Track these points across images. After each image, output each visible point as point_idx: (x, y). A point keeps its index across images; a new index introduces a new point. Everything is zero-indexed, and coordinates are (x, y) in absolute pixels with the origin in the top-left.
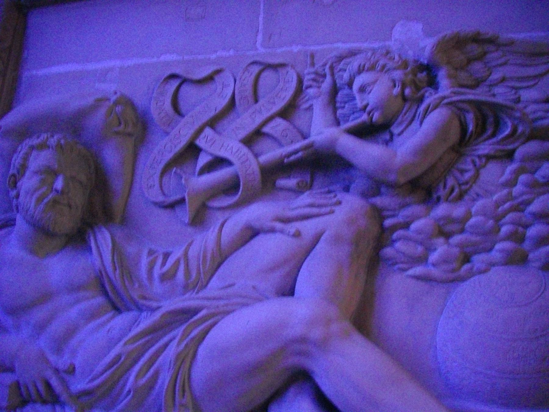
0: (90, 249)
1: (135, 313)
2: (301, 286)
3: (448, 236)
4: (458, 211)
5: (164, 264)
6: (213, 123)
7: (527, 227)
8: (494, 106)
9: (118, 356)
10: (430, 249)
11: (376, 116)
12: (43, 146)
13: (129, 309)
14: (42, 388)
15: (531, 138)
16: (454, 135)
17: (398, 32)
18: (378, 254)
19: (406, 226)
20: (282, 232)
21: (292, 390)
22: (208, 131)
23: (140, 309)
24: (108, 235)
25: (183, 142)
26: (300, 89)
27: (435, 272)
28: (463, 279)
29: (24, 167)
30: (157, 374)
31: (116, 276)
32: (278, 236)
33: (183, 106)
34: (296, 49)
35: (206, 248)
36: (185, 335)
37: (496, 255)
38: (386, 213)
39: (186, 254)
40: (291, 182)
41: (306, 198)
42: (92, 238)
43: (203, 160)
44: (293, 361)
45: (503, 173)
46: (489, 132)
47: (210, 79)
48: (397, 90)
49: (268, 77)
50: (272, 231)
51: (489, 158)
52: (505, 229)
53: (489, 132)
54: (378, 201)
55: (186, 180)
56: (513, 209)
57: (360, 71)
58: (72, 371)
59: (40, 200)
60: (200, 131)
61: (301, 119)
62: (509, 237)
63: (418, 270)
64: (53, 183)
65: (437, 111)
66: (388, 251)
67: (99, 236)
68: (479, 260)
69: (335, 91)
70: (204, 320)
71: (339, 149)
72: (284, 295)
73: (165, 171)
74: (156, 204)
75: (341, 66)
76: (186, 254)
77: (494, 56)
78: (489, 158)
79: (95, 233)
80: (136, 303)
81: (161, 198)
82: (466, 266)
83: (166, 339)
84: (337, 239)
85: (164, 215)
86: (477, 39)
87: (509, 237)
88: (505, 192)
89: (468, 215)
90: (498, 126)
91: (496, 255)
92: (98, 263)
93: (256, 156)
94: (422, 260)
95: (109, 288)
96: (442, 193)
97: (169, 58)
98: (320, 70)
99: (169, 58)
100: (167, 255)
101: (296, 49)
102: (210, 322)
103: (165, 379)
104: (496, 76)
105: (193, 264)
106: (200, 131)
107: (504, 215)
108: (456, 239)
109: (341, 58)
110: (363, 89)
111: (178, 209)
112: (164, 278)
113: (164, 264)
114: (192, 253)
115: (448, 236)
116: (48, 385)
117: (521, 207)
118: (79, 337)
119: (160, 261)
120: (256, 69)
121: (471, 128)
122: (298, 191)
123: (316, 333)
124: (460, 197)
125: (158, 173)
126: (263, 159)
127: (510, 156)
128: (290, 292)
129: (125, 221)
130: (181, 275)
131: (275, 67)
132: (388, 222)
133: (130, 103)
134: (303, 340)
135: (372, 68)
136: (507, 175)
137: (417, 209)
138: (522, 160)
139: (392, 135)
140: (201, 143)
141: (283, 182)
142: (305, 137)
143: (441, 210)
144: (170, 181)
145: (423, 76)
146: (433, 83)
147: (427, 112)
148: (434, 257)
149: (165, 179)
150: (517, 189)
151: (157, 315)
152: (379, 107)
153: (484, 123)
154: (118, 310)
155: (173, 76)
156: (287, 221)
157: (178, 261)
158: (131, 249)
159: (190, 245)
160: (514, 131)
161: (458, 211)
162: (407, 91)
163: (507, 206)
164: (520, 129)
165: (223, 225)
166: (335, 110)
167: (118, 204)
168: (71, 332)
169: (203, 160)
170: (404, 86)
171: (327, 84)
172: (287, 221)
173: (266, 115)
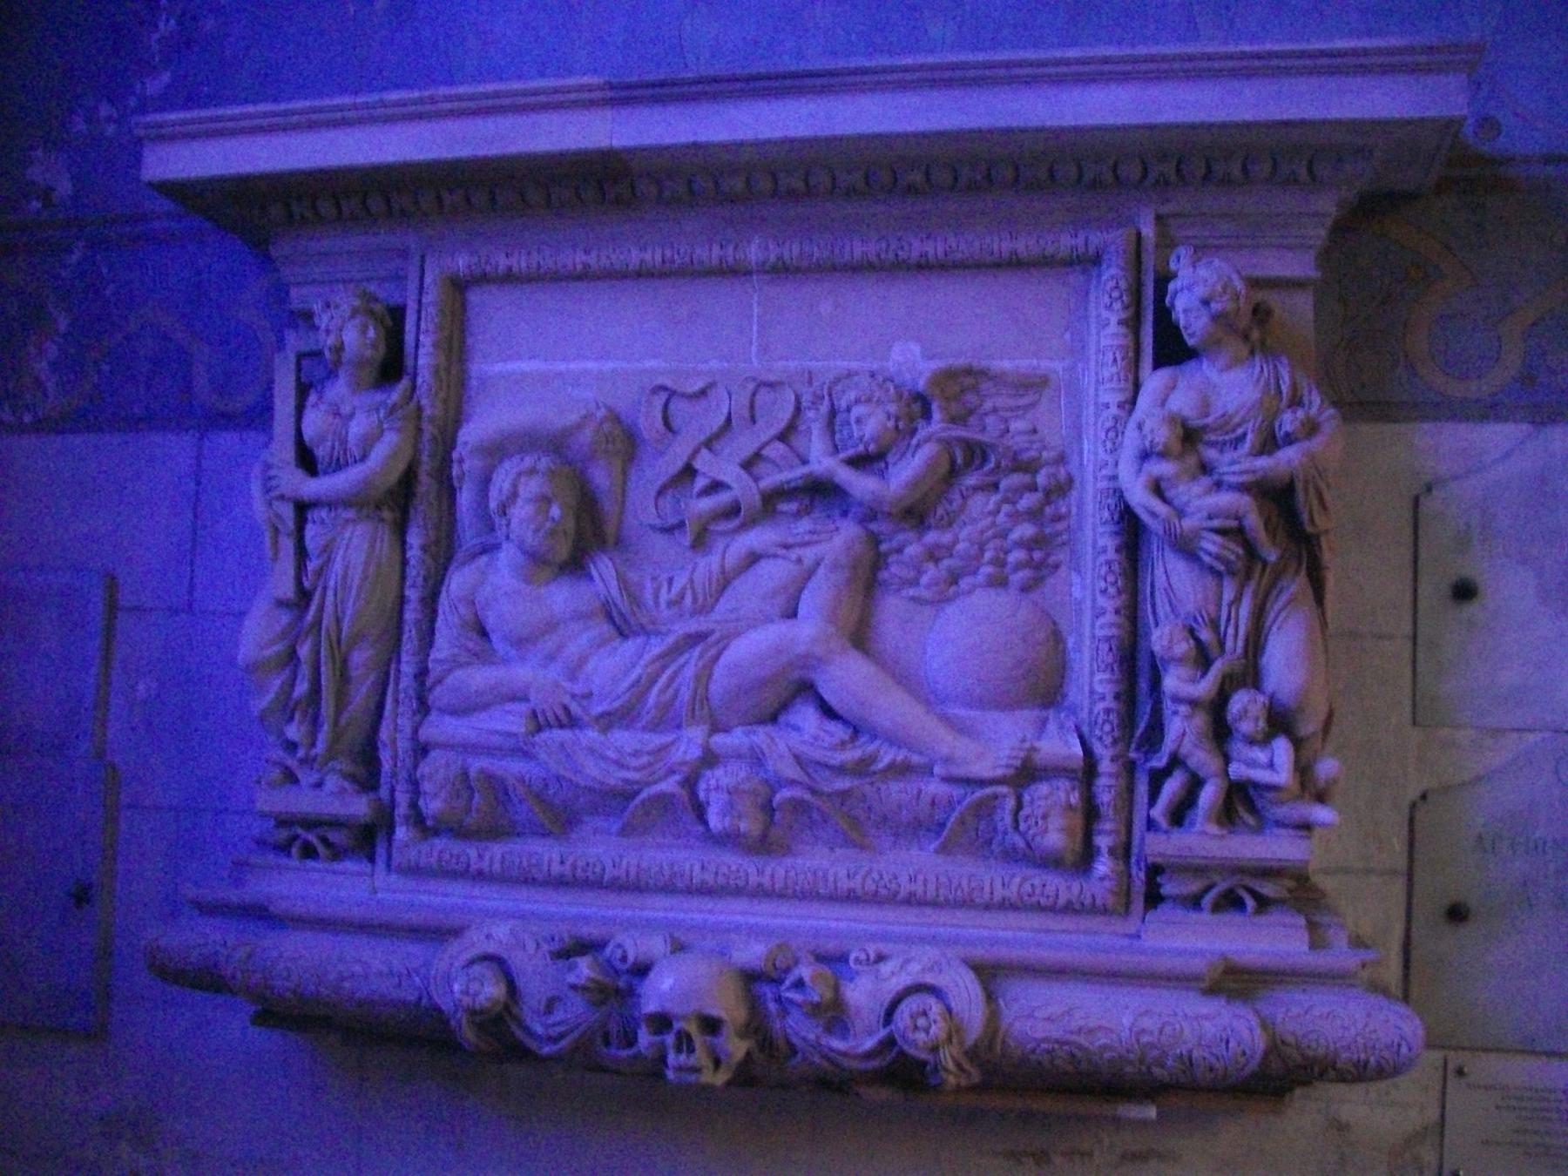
0: (591, 578)
1: (640, 640)
2: (802, 611)
3: (937, 561)
4: (946, 538)
5: (669, 590)
6: (708, 444)
7: (1007, 553)
8: (980, 444)
9: (1122, 518)
10: (920, 572)
11: (872, 447)
12: (532, 471)
13: (636, 634)
14: (560, 713)
15: (1015, 470)
16: (944, 467)
17: (897, 354)
18: (875, 575)
19: (900, 550)
20: (784, 558)
21: (798, 700)
22: (704, 451)
23: (648, 634)
24: (606, 560)
25: (680, 464)
26: (798, 409)
27: (926, 594)
28: (949, 600)
29: (514, 495)
30: (677, 691)
31: (624, 605)
32: (780, 561)
33: (676, 423)
34: (792, 364)
35: (711, 572)
36: (701, 657)
37: (980, 578)
38: (882, 537)
39: (691, 581)
40: (793, 507)
41: (804, 525)
42: (592, 566)
43: (701, 483)
44: (796, 675)
45: (987, 503)
46: (977, 462)
47: (703, 393)
48: (890, 424)
49: (764, 396)
50: (775, 556)
51: (976, 489)
52: (988, 555)
53: (977, 462)
54: (873, 526)
55: (686, 505)
56: (995, 537)
57: (857, 401)
58: (589, 695)
59: (537, 531)
60: (696, 451)
61: (798, 442)
62: (991, 562)
63: (912, 592)
64: (548, 512)
65: (928, 445)
66: (883, 575)
67: (601, 565)
68: (965, 583)
69: (833, 413)
70: (718, 642)
71: (837, 480)
72: (789, 617)
73: (661, 492)
74: (653, 527)
75: (839, 387)
76: (691, 581)
77: (985, 386)
78: (976, 489)
79: (594, 563)
80: (642, 627)
81: (658, 522)
82: (953, 589)
83: (682, 660)
84: (835, 567)
85: (660, 541)
86: (969, 371)
87: (991, 562)
88: (990, 519)
89: (956, 541)
90: (985, 459)
91: (980, 578)
92: (603, 592)
93: (756, 479)
94: (915, 583)
95: (615, 614)
96: (932, 521)
97: (651, 363)
98: (819, 392)
99: (651, 363)
100: (670, 581)
101: (792, 364)
102: (721, 645)
103: (686, 695)
104: (988, 405)
105: (699, 590)
106: (696, 451)
107: (989, 540)
108: (946, 563)
109: (837, 380)
110: (858, 421)
111: (676, 533)
112: (670, 604)
113: (669, 590)
114: (698, 576)
115: (937, 561)
116: (566, 708)
117: (1004, 535)
118: (590, 666)
119: (664, 589)
120: (751, 386)
121: (959, 461)
122: (797, 515)
123: (819, 650)
124: (950, 524)
125: (653, 493)
126: (764, 484)
127: (995, 486)
128: (792, 614)
129: (619, 542)
130: (688, 600)
131: (771, 385)
132: (884, 547)
133: (617, 419)
134: (806, 656)
135: (869, 400)
136: (991, 506)
137: (911, 535)
138: (1006, 491)
139: (887, 464)
140: (697, 465)
141: (784, 507)
142: (805, 462)
143: (931, 537)
144: (667, 503)
145: (916, 408)
146: (927, 415)
147: (918, 446)
148: (924, 580)
149: (661, 502)
150: (1001, 518)
151: (670, 640)
152: (874, 439)
153: (972, 457)
154: (623, 635)
155: (664, 388)
156: (787, 547)
157: (684, 589)
158: (633, 576)
159: (694, 570)
160: (998, 466)
161: (946, 538)
162: (901, 425)
163: (990, 533)
164: (1003, 464)
165: (725, 552)
166: (833, 433)
167: (610, 530)
168: (583, 660)
169: (701, 483)
170: (897, 419)
171: (824, 408)
172: (787, 547)
173: (764, 438)
